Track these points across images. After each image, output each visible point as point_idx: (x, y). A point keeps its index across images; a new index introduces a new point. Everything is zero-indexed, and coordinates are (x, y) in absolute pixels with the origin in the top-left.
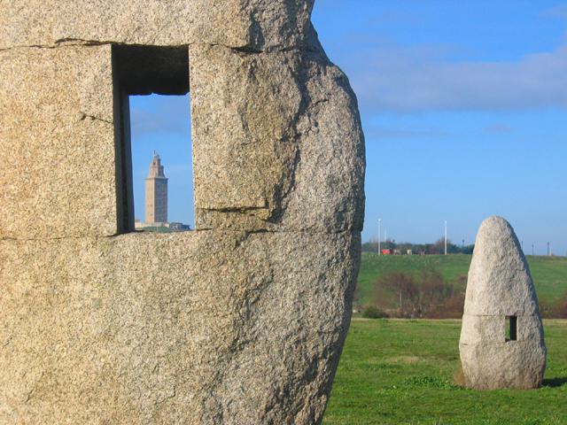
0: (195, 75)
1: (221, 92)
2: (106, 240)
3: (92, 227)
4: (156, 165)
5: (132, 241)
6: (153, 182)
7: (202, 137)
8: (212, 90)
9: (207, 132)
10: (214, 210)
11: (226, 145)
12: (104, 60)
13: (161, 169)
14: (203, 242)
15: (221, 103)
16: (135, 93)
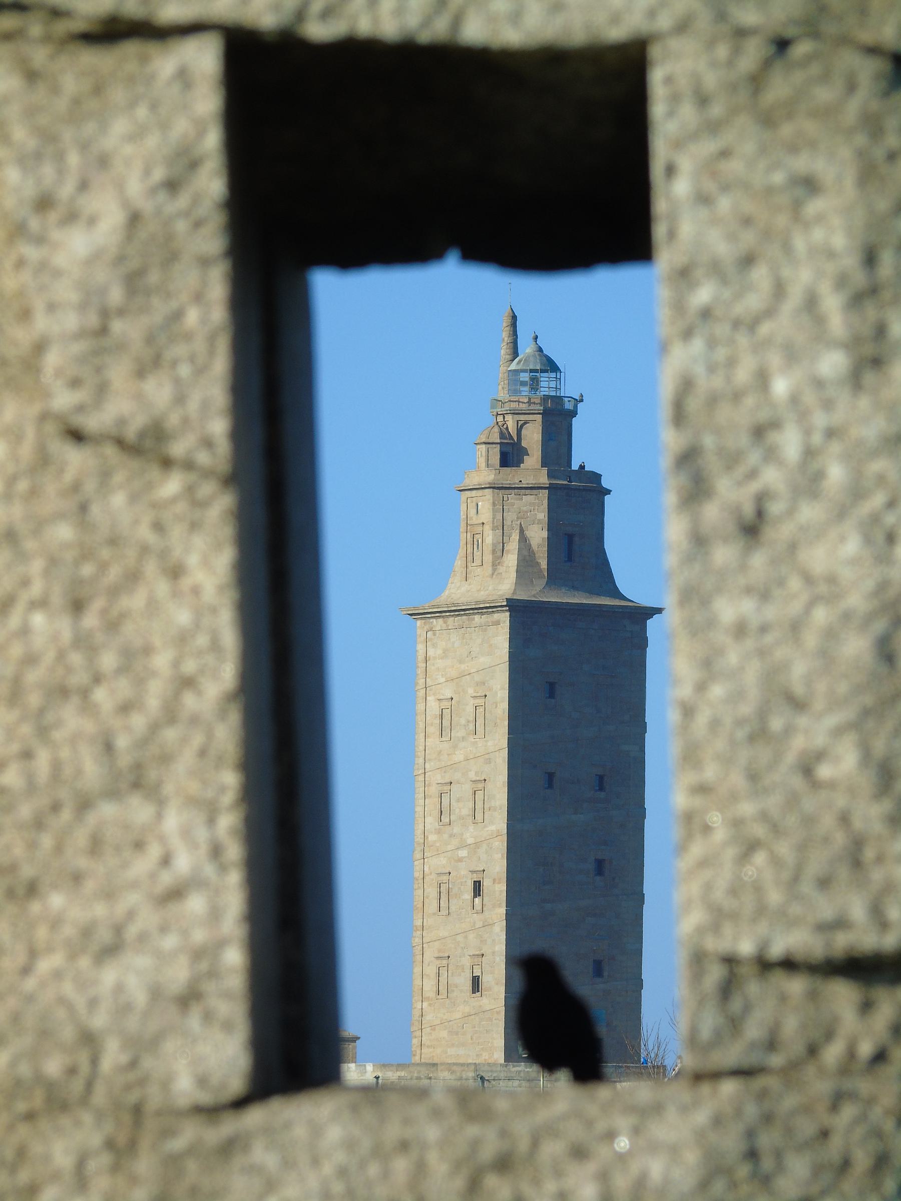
0: (676, 191)
1: (833, 304)
2: (189, 1134)
3: (113, 1055)
4: (532, 470)
5: (334, 1134)
6: (496, 640)
7: (723, 554)
8: (779, 290)
9: (752, 528)
10: (789, 964)
11: (857, 600)
12: (181, 127)
13: (577, 502)
14: (731, 1142)
15: (832, 363)
16: (351, 256)
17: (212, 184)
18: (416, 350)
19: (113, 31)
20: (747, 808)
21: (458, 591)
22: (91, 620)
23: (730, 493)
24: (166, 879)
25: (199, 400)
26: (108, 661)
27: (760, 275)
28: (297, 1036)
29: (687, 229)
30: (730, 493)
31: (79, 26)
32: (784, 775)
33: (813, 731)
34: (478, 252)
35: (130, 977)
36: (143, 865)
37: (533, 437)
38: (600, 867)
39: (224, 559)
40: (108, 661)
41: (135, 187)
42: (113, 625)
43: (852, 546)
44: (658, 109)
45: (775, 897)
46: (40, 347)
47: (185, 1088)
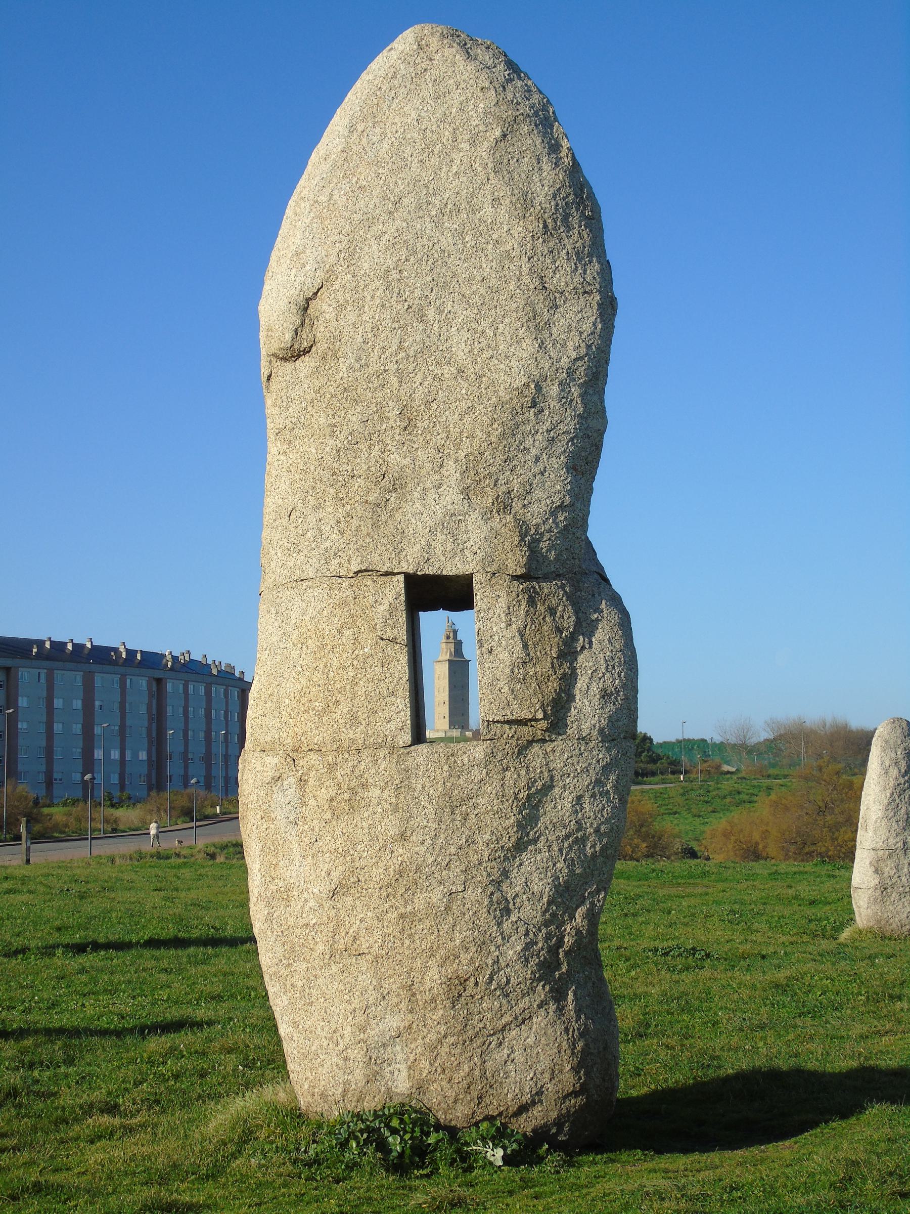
0: (477, 598)
1: (503, 615)
2: (402, 750)
4: (451, 640)
6: (446, 666)
10: (498, 722)
13: (458, 645)
14: (489, 751)
15: (503, 625)
18: (434, 622)
19: (387, 574)
20: (491, 697)
21: (440, 658)
22: (385, 669)
23: (487, 646)
25: (402, 634)
26: (388, 675)
27: (491, 611)
28: (419, 736)
30: (487, 646)
32: (496, 691)
33: (501, 684)
35: (392, 726)
36: (394, 708)
37: (451, 635)
40: (388, 675)
41: (391, 599)
42: (388, 669)
43: (506, 655)
45: (495, 711)
46: (376, 625)
47: (401, 744)
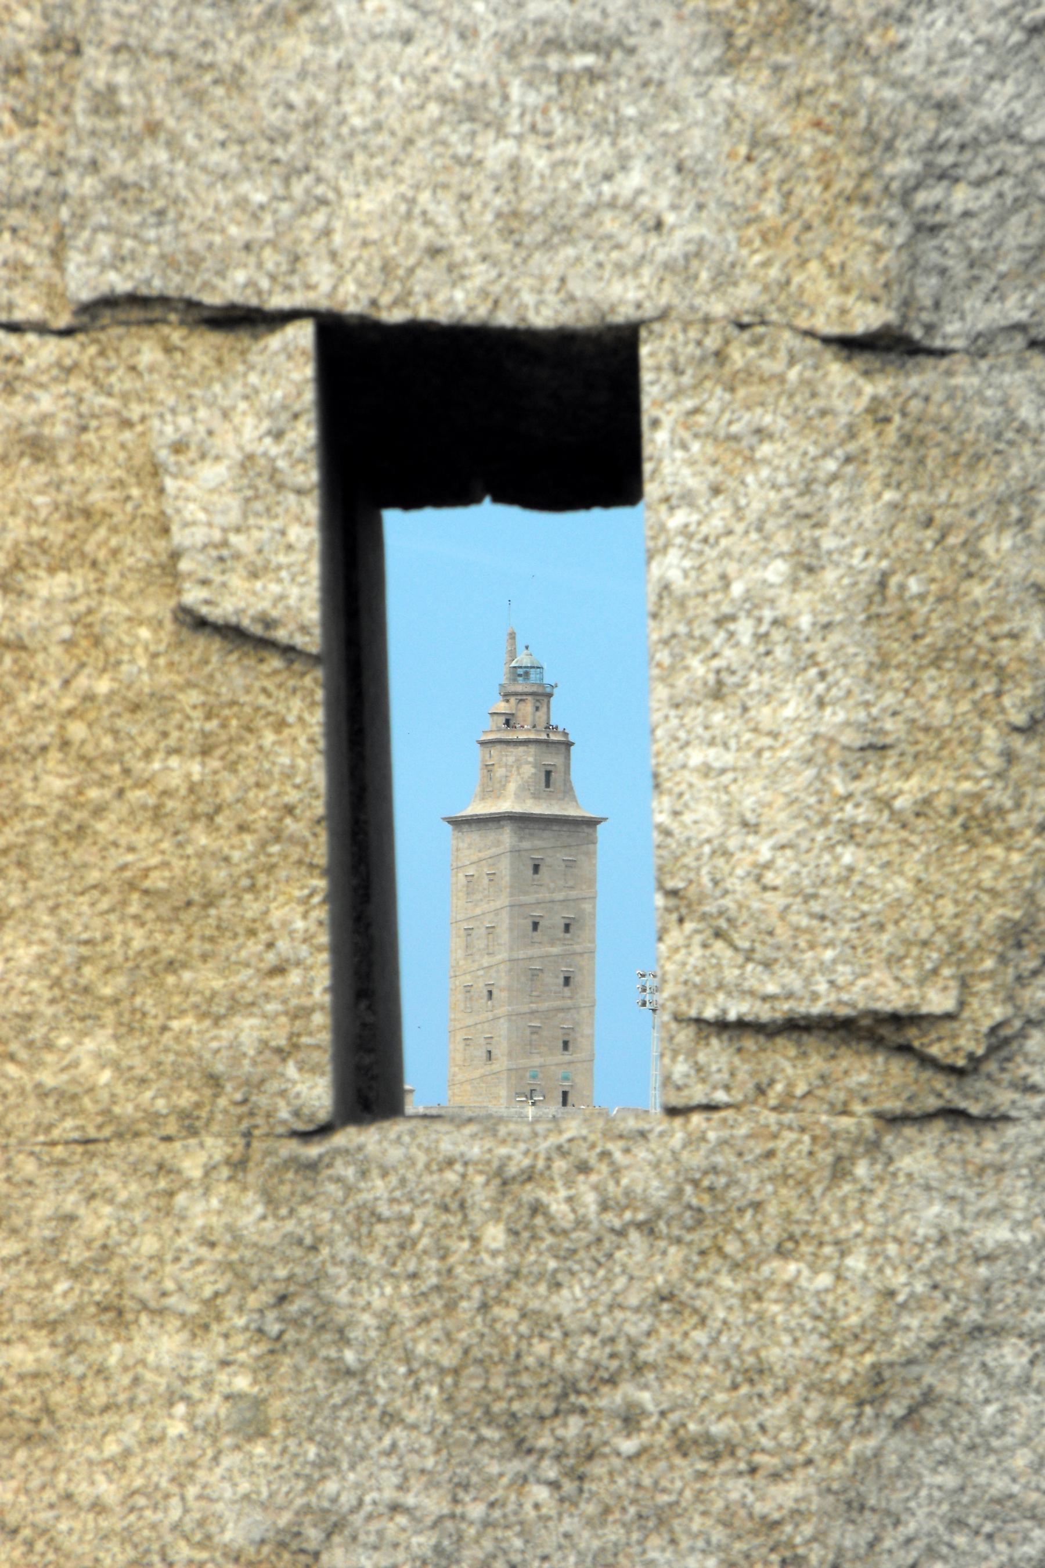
16: (410, 502)
17: (306, 433)
24: (271, 958)
28: (370, 1083)
29: (667, 468)
31: (206, 314)
34: (502, 497)
38: (567, 981)
39: (317, 717)
44: (646, 377)
